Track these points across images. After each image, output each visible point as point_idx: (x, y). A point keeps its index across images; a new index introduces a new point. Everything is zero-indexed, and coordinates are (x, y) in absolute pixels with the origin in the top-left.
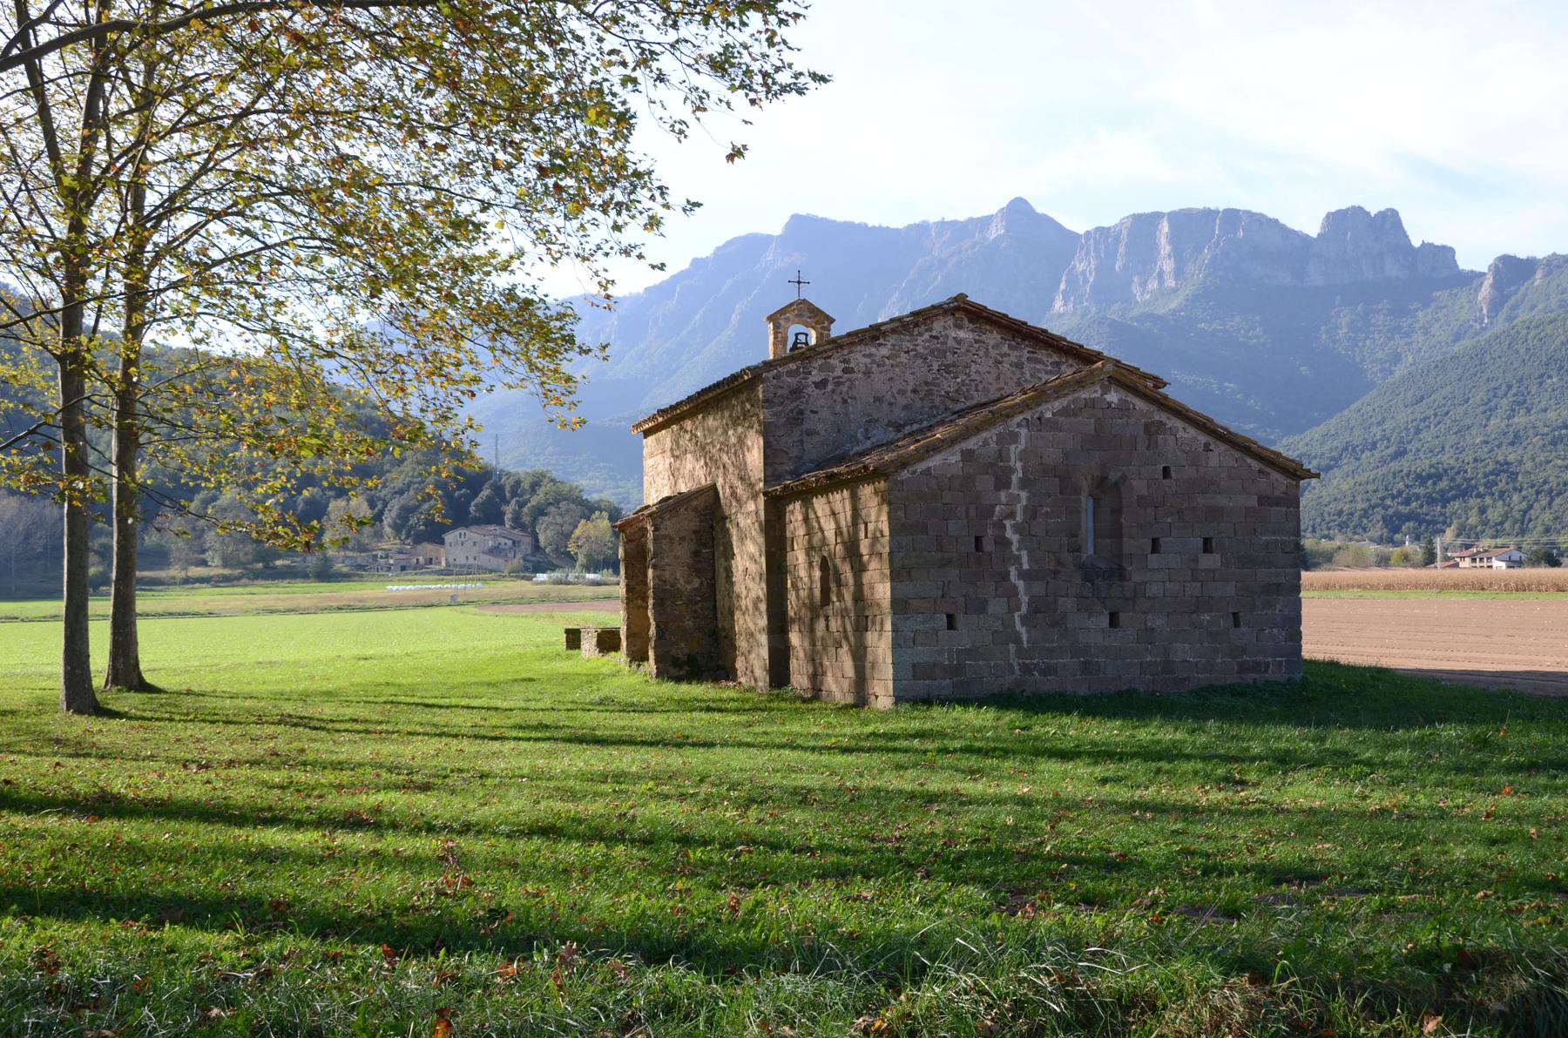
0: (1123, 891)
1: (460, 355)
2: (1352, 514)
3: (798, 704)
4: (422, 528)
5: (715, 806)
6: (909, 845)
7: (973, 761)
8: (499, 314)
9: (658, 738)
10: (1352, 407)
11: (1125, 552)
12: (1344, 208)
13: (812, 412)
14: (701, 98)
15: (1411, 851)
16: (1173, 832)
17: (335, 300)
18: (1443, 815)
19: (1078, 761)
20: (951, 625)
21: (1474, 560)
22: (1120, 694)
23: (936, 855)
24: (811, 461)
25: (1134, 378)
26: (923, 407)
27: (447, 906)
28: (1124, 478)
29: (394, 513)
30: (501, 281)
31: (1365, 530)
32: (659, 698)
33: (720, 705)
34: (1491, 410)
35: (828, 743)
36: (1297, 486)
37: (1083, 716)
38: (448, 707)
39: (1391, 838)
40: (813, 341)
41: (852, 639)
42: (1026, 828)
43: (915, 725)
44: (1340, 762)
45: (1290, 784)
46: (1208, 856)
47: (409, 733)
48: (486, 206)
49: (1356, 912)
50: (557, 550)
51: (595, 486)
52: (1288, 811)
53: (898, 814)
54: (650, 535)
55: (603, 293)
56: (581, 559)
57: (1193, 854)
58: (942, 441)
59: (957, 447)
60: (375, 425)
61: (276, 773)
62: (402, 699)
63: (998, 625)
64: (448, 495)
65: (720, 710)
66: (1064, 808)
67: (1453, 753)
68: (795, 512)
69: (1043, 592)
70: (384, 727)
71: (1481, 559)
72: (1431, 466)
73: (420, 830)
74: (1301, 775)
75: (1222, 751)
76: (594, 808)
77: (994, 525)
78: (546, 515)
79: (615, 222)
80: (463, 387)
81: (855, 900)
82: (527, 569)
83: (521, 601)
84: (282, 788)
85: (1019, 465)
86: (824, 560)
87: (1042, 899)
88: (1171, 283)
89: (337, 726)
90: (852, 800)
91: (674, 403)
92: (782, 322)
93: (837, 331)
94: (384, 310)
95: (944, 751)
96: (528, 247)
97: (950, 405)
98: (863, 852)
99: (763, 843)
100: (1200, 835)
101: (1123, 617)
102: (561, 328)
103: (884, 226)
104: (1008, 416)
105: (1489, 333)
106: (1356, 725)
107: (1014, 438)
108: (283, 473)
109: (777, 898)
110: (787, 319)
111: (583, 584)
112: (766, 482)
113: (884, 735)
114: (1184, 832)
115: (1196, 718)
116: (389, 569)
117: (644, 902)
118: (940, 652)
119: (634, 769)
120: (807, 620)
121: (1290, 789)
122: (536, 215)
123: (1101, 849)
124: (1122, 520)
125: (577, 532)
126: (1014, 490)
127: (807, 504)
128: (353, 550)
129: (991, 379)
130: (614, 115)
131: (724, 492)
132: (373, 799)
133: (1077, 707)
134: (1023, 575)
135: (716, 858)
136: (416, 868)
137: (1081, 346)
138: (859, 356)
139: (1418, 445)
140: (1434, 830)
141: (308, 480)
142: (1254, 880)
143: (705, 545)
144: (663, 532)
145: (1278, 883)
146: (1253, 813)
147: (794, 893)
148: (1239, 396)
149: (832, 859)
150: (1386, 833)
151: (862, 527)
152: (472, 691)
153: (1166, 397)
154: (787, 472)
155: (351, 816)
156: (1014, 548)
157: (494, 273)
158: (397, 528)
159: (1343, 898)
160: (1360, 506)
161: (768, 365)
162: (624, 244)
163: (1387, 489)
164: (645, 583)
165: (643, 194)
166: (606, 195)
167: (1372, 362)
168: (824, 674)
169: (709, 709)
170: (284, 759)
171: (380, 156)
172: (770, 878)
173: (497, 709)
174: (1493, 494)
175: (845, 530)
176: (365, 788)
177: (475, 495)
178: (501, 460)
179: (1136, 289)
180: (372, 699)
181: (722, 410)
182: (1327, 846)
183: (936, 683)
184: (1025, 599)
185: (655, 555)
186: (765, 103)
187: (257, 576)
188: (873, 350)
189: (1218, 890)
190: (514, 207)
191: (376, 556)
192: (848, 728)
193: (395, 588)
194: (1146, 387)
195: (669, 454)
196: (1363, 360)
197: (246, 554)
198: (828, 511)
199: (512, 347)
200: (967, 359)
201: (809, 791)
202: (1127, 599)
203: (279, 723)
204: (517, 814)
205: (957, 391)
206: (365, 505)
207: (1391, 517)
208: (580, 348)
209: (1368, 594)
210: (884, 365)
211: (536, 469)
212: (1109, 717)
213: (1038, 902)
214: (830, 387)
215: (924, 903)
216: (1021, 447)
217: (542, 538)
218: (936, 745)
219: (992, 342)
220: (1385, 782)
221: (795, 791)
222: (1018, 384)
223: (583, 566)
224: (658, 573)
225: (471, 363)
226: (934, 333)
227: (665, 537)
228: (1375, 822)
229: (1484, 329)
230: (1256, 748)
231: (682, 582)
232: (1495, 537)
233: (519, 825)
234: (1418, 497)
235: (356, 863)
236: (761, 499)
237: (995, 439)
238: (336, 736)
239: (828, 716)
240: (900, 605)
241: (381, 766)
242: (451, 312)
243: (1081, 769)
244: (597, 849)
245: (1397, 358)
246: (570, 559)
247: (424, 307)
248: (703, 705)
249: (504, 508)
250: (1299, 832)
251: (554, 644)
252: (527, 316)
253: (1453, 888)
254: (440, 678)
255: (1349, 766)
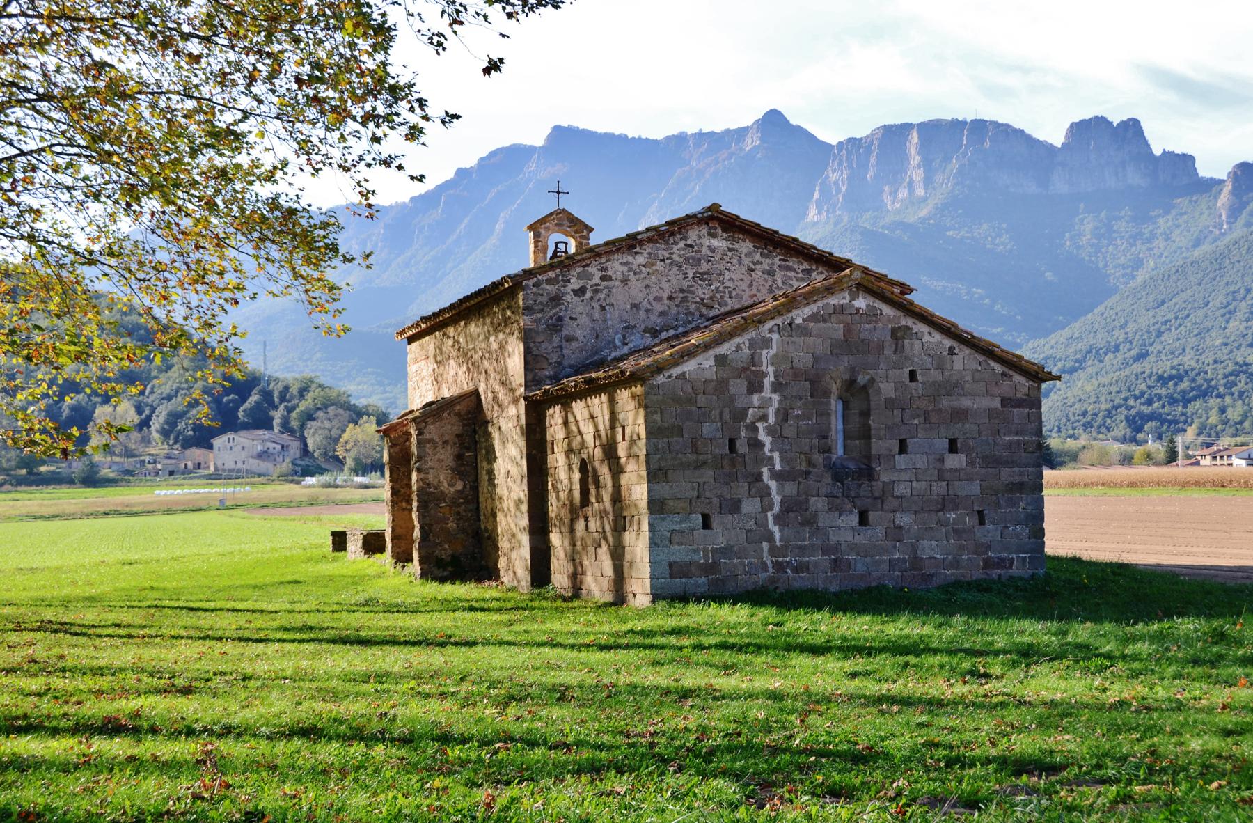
0: (868, 783)
1: (224, 263)
2: (1096, 414)
3: (559, 603)
4: (191, 433)
5: (475, 705)
6: (663, 740)
7: (727, 657)
8: (262, 223)
9: (421, 638)
10: (1096, 311)
11: (873, 452)
12: (1087, 118)
13: (571, 318)
14: (458, 12)
15: (1149, 742)
16: (918, 724)
17: (95, 208)
18: (1180, 707)
19: (828, 655)
20: (707, 524)
21: (1215, 458)
22: (870, 590)
23: (688, 750)
24: (571, 366)
25: (882, 284)
26: (678, 313)
27: (203, 811)
28: (872, 381)
29: (162, 419)
30: (265, 191)
31: (1108, 429)
32: (423, 599)
33: (482, 604)
34: (1230, 313)
35: (587, 641)
36: (1039, 388)
37: (834, 611)
38: (213, 610)
39: (1129, 730)
40: (572, 250)
41: (611, 539)
42: (776, 722)
43: (671, 623)
44: (1083, 652)
45: (1033, 677)
46: (951, 748)
47: (173, 637)
48: (246, 115)
49: (1094, 803)
50: (325, 454)
51: (363, 392)
52: (1030, 703)
53: (653, 710)
54: (414, 440)
55: (365, 203)
56: (350, 463)
57: (937, 745)
58: (697, 346)
59: (711, 352)
60: (142, 332)
61: (34, 680)
62: (166, 603)
63: (751, 525)
64: (217, 401)
65: (483, 610)
66: (814, 702)
67: (1191, 646)
68: (555, 416)
69: (795, 492)
70: (147, 631)
71: (1222, 457)
72: (1173, 368)
73: (180, 733)
74: (1043, 668)
75: (967, 646)
76: (355, 709)
77: (747, 427)
78: (314, 419)
79: (374, 134)
80: (228, 294)
81: (608, 795)
82: (296, 473)
83: (290, 504)
84: (39, 695)
85: (771, 370)
86: (583, 462)
87: (790, 792)
88: (920, 192)
89: (99, 631)
90: (609, 697)
91: (436, 310)
92: (542, 231)
93: (595, 240)
94: (146, 218)
95: (700, 647)
96: (292, 158)
97: (705, 311)
98: (618, 748)
99: (521, 740)
100: (944, 728)
101: (872, 516)
102: (324, 237)
103: (643, 137)
104: (760, 322)
105: (1228, 238)
106: (1097, 619)
107: (766, 343)
108: (43, 380)
109: (532, 794)
110: (547, 229)
111: (351, 487)
112: (526, 387)
113: (642, 632)
114: (929, 725)
115: (942, 613)
116: (157, 474)
117: (401, 801)
118: (696, 551)
119: (396, 669)
120: (567, 521)
121: (1032, 682)
122: (298, 125)
123: (849, 742)
124: (871, 422)
125: (345, 436)
126: (766, 393)
127: (566, 407)
128: (120, 455)
129: (744, 286)
130: (372, 27)
131: (486, 398)
132: (133, 704)
133: (828, 604)
134: (775, 476)
135: (473, 756)
136: (173, 772)
137: (831, 254)
138: (616, 264)
139: (1160, 347)
140: (1171, 721)
141: (72, 387)
142: (996, 771)
143: (468, 449)
144: (427, 436)
145: (1018, 774)
146: (996, 705)
147: (548, 789)
148: (986, 301)
149: (587, 754)
150: (1124, 724)
151: (619, 430)
152: (238, 594)
153: (912, 303)
154: (547, 377)
155: (110, 721)
156: (766, 449)
157: (257, 183)
158: (165, 433)
159: (1080, 789)
160: (1105, 406)
161: (528, 273)
162: (385, 155)
163: (1129, 390)
164: (410, 486)
165: (402, 107)
166: (368, 107)
167: (1115, 267)
168: (583, 573)
169: (472, 609)
170: (42, 665)
171: (139, 64)
172: (526, 774)
173: (262, 611)
174: (1233, 394)
175: (603, 433)
176: (125, 693)
177: (244, 400)
178: (269, 366)
179: (887, 199)
180: (136, 604)
181: (484, 317)
182: (1067, 737)
183: (692, 581)
184: (777, 499)
185: (420, 458)
186: (522, 17)
187: (20, 482)
188: (630, 258)
189: (960, 782)
190: (277, 118)
191: (144, 461)
192: (607, 626)
193: (163, 492)
194: (892, 293)
195: (432, 359)
196: (1106, 265)
197: (9, 460)
198: (587, 415)
199: (275, 255)
200: (721, 267)
201: (567, 688)
202: (876, 498)
203: (39, 629)
204: (278, 716)
205: (711, 298)
206: (132, 411)
207: (1134, 417)
208: (344, 256)
209: (1112, 492)
210: (640, 272)
211: (305, 375)
212: (859, 613)
213: (787, 795)
214: (588, 295)
215: (675, 797)
216: (773, 351)
217: (310, 442)
218: (693, 640)
219: (745, 250)
220: (1124, 675)
221: (554, 688)
222: (771, 291)
223: (351, 469)
224: (422, 476)
225: (236, 271)
226: (689, 242)
227: (429, 441)
228: (1114, 713)
229: (1223, 234)
230: (1001, 642)
231: (445, 484)
232: (1235, 435)
233: (280, 726)
234: (1160, 398)
235: (112, 770)
236: (522, 403)
237: (747, 344)
238: (98, 641)
239: (587, 614)
240: (657, 506)
241: (143, 670)
242: (214, 221)
243: (831, 663)
244: (358, 749)
245: (1138, 263)
246: (339, 462)
247: (187, 215)
248: (466, 605)
249: (272, 413)
250: (1040, 724)
251: (321, 546)
252: (290, 226)
253: (1189, 778)
254: (206, 582)
255: (1090, 659)
